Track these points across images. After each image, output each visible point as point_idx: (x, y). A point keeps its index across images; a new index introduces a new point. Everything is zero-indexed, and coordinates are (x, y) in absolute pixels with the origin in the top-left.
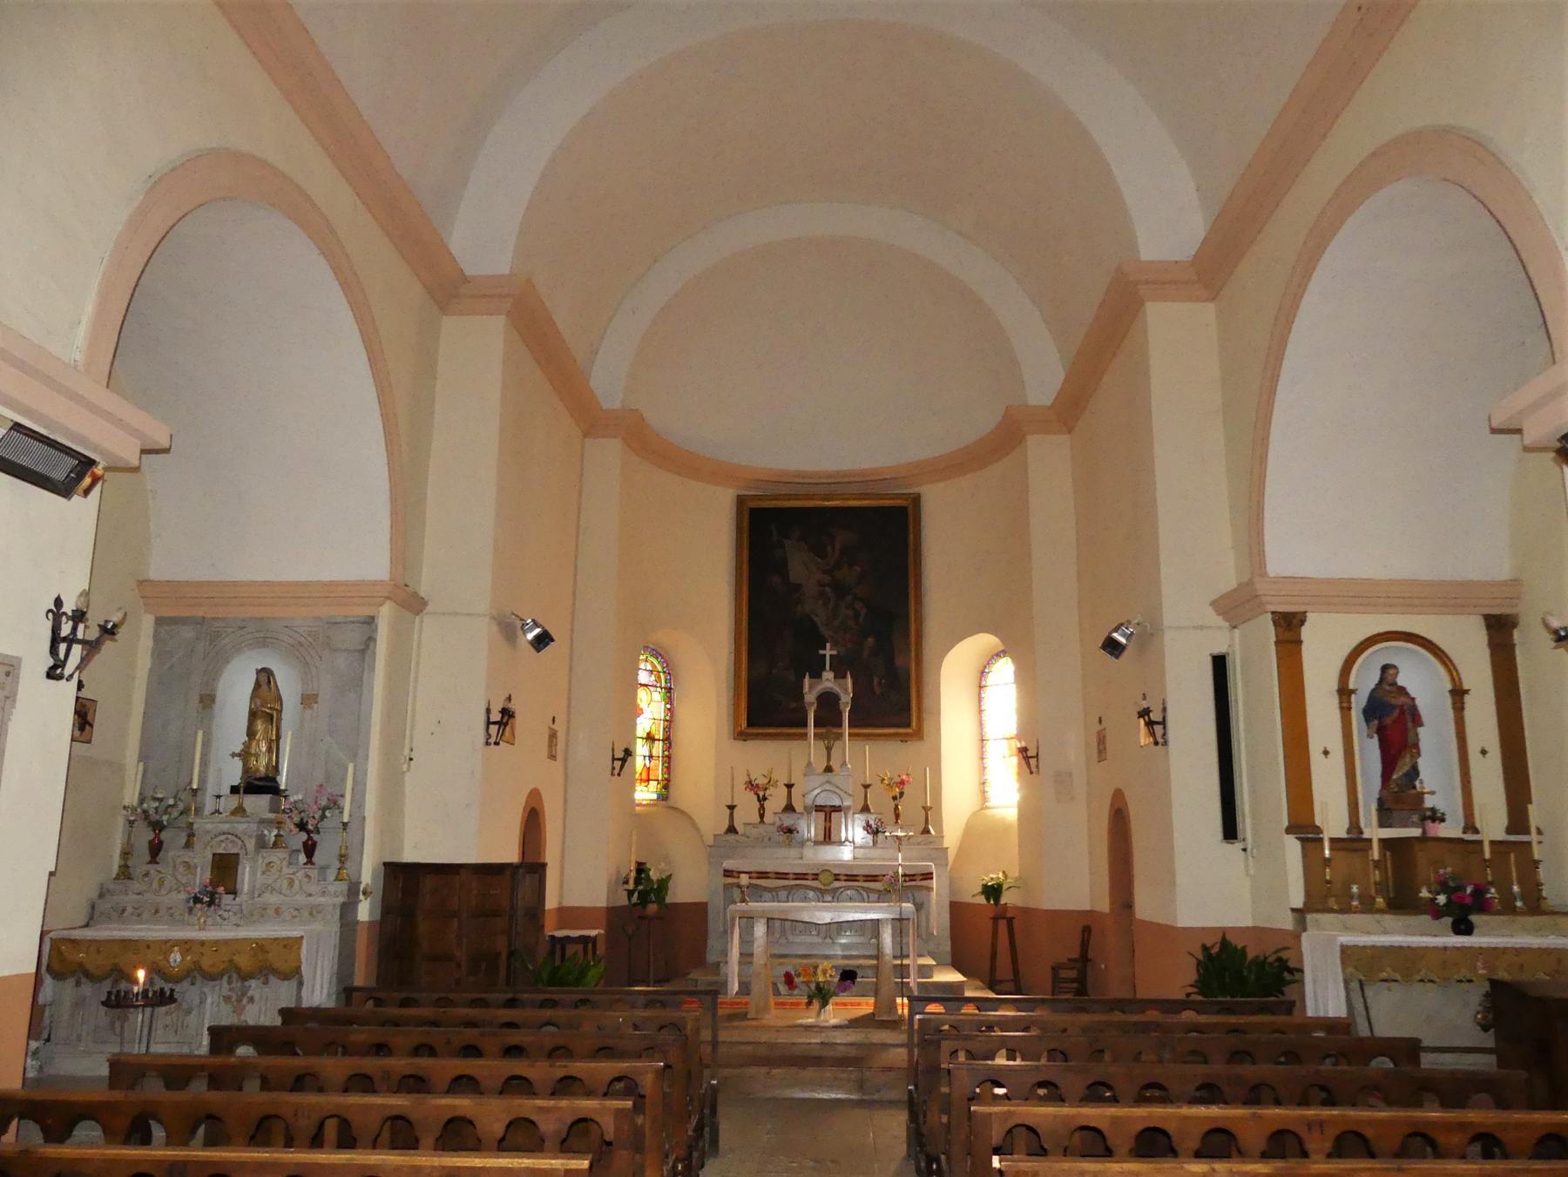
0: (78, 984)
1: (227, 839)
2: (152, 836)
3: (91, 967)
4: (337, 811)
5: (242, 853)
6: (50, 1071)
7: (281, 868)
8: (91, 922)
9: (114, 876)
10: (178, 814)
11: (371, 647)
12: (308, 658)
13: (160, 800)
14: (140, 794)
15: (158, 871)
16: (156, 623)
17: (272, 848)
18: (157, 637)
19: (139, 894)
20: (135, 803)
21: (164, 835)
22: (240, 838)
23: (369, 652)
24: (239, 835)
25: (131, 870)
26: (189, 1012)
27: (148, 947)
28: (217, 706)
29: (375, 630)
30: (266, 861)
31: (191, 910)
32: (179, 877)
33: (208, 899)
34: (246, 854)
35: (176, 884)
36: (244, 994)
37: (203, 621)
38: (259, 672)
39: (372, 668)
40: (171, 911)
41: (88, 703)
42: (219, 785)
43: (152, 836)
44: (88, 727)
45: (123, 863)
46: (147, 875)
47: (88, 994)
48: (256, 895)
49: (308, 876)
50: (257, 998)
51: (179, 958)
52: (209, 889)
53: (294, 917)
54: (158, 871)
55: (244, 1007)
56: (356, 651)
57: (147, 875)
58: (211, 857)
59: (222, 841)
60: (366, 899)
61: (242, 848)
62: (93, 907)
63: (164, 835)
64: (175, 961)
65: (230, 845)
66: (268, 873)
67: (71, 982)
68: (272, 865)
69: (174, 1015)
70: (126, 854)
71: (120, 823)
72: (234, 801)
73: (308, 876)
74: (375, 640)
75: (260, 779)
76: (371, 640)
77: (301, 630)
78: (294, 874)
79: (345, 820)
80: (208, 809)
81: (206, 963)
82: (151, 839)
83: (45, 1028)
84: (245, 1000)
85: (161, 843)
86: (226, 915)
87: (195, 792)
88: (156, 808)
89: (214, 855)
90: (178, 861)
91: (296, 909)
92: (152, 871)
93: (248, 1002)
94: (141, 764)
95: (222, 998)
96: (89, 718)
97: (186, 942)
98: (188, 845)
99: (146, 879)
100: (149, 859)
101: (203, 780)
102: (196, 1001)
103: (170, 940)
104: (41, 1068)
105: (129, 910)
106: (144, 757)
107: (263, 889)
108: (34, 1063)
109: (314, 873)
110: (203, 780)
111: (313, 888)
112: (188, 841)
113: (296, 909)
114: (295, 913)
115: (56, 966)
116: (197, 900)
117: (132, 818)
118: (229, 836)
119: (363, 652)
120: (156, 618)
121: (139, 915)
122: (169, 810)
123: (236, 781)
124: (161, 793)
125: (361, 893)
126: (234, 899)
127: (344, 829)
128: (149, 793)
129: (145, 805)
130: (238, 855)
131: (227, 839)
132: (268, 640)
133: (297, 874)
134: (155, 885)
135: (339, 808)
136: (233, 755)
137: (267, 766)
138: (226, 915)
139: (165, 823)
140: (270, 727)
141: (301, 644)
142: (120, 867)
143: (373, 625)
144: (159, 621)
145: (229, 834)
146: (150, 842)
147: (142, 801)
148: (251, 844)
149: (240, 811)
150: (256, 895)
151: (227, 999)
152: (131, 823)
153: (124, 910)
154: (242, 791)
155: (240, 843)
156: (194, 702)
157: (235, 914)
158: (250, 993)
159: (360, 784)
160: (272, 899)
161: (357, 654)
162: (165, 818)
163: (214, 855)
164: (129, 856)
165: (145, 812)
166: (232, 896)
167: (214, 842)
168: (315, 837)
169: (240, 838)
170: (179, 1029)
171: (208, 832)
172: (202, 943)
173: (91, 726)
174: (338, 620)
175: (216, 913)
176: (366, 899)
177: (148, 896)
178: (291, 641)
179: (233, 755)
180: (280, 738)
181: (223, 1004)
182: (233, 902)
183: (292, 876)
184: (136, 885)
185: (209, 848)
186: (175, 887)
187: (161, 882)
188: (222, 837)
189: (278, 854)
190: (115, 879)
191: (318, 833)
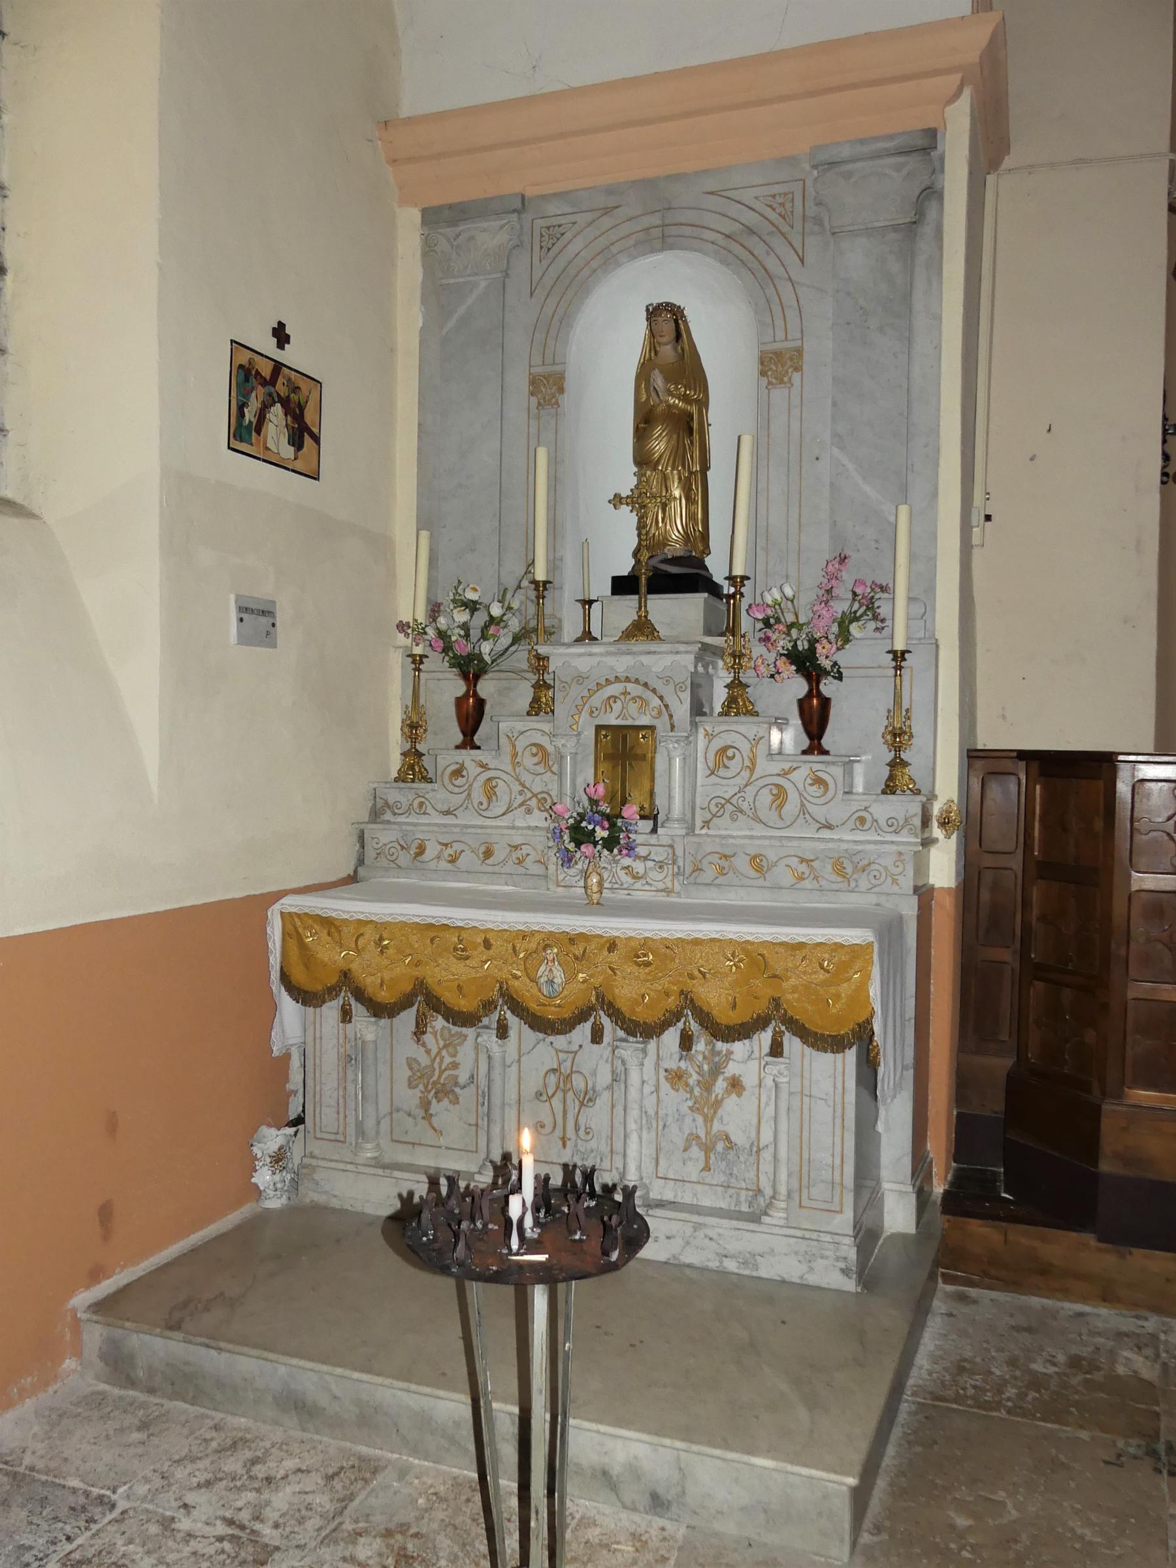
0: (346, 1015)
1: (625, 693)
2: (460, 688)
3: (370, 983)
4: (872, 625)
5: (662, 725)
6: (311, 1195)
7: (753, 761)
8: (361, 870)
9: (395, 774)
10: (510, 640)
11: (931, 214)
12: (772, 264)
13: (472, 607)
14: (429, 600)
15: (482, 766)
16: (425, 222)
17: (725, 713)
18: (428, 249)
19: (447, 813)
20: (421, 617)
21: (485, 688)
22: (654, 691)
23: (927, 229)
24: (653, 683)
25: (426, 761)
26: (587, 1099)
27: (487, 944)
28: (566, 400)
29: (937, 168)
30: (717, 744)
31: (568, 860)
32: (527, 778)
33: (605, 834)
34: (673, 727)
35: (521, 793)
36: (716, 1071)
37: (523, 204)
38: (654, 313)
39: (936, 266)
40: (518, 854)
41: (303, 384)
42: (586, 583)
43: (460, 688)
44: (307, 440)
45: (408, 746)
46: (458, 773)
47: (370, 1037)
48: (698, 823)
49: (819, 781)
50: (749, 1081)
51: (559, 977)
52: (605, 808)
53: (801, 878)
54: (482, 766)
55: (718, 1103)
56: (895, 228)
57: (458, 773)
58: (590, 733)
59: (615, 698)
60: (948, 837)
61: (660, 713)
62: (361, 838)
63: (485, 688)
64: (551, 982)
65: (633, 708)
66: (722, 772)
67: (331, 1011)
68: (730, 753)
69: (556, 1103)
70: (413, 728)
71: (397, 665)
72: (626, 609)
73: (819, 781)
74: (940, 196)
75: (675, 561)
76: (931, 193)
77: (747, 196)
78: (785, 774)
79: (899, 646)
80: (571, 627)
81: (625, 992)
82: (801, 695)
83: (295, 1092)
84: (720, 1085)
85: (480, 704)
86: (639, 867)
87: (541, 588)
88: (465, 627)
89: (599, 728)
90: (521, 744)
91: (802, 860)
92: (468, 764)
93: (728, 1092)
94: (424, 534)
95: (662, 1074)
96: (309, 417)
97: (572, 940)
98: (537, 708)
99: (460, 781)
100: (459, 738)
101: (554, 564)
102: (604, 1077)
103: (533, 933)
104: (295, 1184)
105: (431, 851)
106: (426, 521)
107: (714, 810)
108: (277, 1177)
109: (833, 773)
110: (554, 564)
111: (837, 811)
112: (536, 700)
113: (802, 860)
114: (803, 868)
115: (299, 976)
116: (580, 836)
117: (418, 650)
118: (630, 687)
119: (912, 228)
120: (425, 212)
121: (453, 860)
122: (492, 630)
123: (624, 567)
124: (475, 590)
125: (935, 824)
126: (654, 830)
127: (898, 668)
128: (446, 598)
129: (442, 621)
130: (652, 728)
131: (625, 693)
132: (673, 230)
133: (794, 776)
134: (478, 794)
135: (875, 617)
136: (617, 500)
137: (687, 538)
138: (639, 867)
139: (487, 658)
140: (687, 442)
141: (751, 231)
142: (404, 754)
143: (934, 154)
144: (432, 217)
145: (628, 680)
146: (460, 702)
147: (434, 610)
148: (682, 709)
149: (642, 629)
150: (895, 889)
151: (676, 1078)
152: (417, 661)
153: (421, 850)
154: (643, 589)
155: (656, 702)
156: (519, 382)
157: (661, 866)
158: (732, 1069)
159: (922, 560)
160: (736, 832)
161: (892, 236)
162: (486, 648)
163: (599, 728)
164: (421, 731)
165: (442, 635)
166: (649, 824)
167: (597, 700)
168: (828, 687)
169: (654, 691)
170: (570, 1132)
171: (580, 679)
172: (612, 945)
173: (316, 439)
174: (846, 152)
175: (617, 862)
176: (948, 837)
177: (467, 818)
178: (727, 227)
179: (617, 500)
180: (708, 468)
181: (665, 1086)
182: (653, 839)
183: (780, 781)
184: (439, 794)
185: (585, 713)
186: (520, 799)
187: (490, 791)
188: (615, 689)
189: (742, 728)
190: (396, 780)
191: (840, 677)
